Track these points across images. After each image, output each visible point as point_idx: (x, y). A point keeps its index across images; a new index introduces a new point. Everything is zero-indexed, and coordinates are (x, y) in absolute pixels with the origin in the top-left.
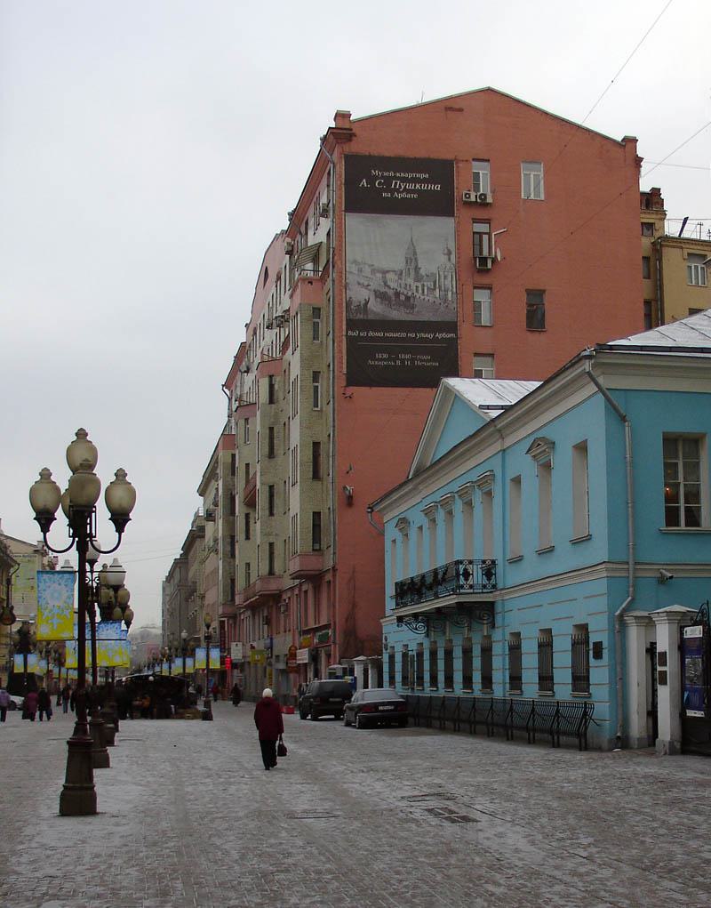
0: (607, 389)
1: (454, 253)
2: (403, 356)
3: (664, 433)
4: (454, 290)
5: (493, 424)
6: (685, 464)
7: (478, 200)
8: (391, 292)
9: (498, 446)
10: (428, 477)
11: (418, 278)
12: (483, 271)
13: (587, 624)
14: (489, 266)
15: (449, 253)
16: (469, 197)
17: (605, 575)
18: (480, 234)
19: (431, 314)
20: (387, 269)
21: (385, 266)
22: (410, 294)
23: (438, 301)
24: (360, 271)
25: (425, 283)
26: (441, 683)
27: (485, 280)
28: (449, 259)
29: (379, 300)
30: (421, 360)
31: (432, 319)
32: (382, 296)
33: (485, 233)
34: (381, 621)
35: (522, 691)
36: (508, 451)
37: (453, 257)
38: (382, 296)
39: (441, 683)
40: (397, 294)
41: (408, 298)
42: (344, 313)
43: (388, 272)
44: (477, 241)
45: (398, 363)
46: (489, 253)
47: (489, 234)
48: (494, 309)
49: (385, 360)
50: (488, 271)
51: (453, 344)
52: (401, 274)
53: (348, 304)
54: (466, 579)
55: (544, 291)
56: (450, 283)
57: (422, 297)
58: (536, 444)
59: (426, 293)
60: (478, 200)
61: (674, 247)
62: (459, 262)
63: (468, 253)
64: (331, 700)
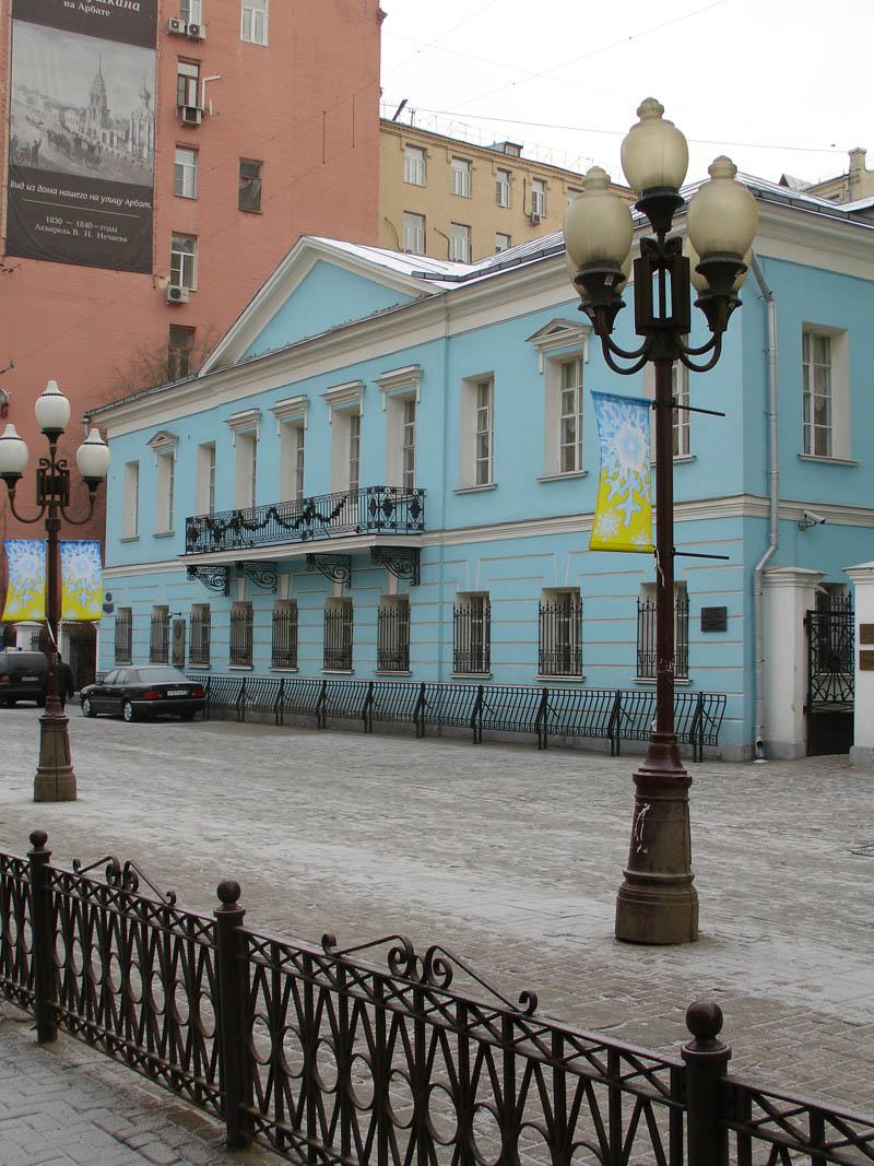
0: (758, 256)
1: (153, 95)
2: (82, 225)
3: (803, 323)
4: (152, 145)
5: (443, 298)
6: (815, 367)
7: (189, 32)
8: (69, 137)
9: (439, 330)
10: (238, 377)
11: (106, 124)
12: (190, 126)
13: (686, 582)
14: (199, 120)
15: (148, 96)
16: (177, 27)
17: (741, 513)
18: (187, 78)
19: (120, 174)
20: (67, 105)
21: (63, 100)
22: (94, 143)
23: (130, 158)
24: (30, 101)
25: (115, 132)
26: (262, 653)
27: (191, 138)
28: (147, 104)
29: (53, 144)
30: (105, 233)
31: (122, 181)
32: (58, 141)
36: (454, 339)
37: (152, 102)
38: (58, 141)
39: (262, 653)
40: (78, 141)
41: (91, 148)
42: (6, 156)
43: (67, 109)
45: (75, 232)
47: (197, 79)
48: (197, 175)
49: (57, 226)
50: (195, 126)
51: (147, 216)
52: (84, 115)
53: (13, 144)
54: (388, 514)
55: (261, 163)
56: (146, 135)
57: (110, 150)
58: (161, 436)
59: (115, 144)
60: (189, 32)
61: (390, 133)
62: (158, 111)
63: (172, 100)
64: (24, 679)
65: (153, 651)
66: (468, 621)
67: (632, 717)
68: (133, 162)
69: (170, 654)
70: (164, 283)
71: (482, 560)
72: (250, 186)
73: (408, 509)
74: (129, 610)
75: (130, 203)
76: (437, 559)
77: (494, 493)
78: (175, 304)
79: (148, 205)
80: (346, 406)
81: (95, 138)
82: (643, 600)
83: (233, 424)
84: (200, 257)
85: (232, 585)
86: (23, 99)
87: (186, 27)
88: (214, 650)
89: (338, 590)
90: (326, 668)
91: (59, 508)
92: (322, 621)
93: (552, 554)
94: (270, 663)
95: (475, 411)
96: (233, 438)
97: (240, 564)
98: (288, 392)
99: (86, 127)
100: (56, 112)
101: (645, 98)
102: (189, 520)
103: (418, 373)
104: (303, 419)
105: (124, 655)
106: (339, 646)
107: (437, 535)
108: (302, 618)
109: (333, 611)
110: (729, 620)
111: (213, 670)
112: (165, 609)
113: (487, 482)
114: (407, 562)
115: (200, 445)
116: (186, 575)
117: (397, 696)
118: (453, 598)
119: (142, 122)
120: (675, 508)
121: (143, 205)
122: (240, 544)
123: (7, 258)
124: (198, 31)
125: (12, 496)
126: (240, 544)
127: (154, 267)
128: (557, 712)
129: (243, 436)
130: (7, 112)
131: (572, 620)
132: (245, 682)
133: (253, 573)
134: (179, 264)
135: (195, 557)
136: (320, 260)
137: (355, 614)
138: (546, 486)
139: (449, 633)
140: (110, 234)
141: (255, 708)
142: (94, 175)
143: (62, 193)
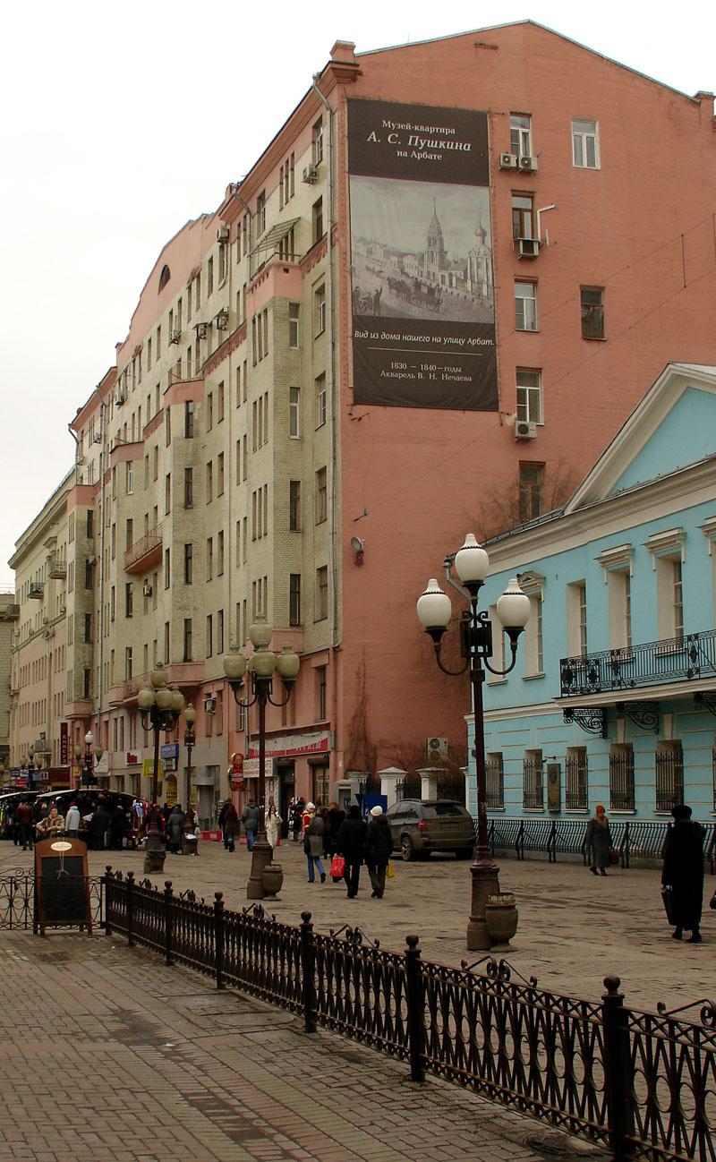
1: (488, 231)
4: (491, 281)
7: (521, 166)
8: (409, 283)
11: (444, 265)
12: (528, 259)
14: (536, 252)
15: (483, 234)
16: (509, 162)
18: (521, 211)
21: (402, 246)
22: (434, 285)
23: (470, 297)
24: (370, 252)
25: (453, 272)
27: (527, 271)
28: (483, 242)
29: (394, 291)
30: (450, 374)
31: (462, 320)
32: (398, 287)
33: (527, 210)
35: (635, 811)
37: (488, 239)
38: (398, 287)
40: (418, 285)
41: (431, 291)
43: (406, 255)
45: (420, 376)
47: (532, 211)
49: (403, 371)
50: (533, 259)
51: (489, 355)
52: (422, 259)
55: (602, 289)
56: (484, 273)
60: (521, 166)
69: (546, 799)
70: (511, 420)
72: (592, 315)
74: (499, 755)
75: (472, 342)
78: (523, 441)
79: (489, 342)
83: (604, 561)
84: (546, 390)
85: (610, 731)
86: (362, 250)
87: (517, 160)
91: (482, 659)
94: (654, 807)
97: (620, 705)
98: (665, 525)
99: (425, 270)
100: (394, 259)
102: (563, 662)
108: (688, 758)
109: (664, 754)
111: (507, 813)
112: (538, 753)
116: (562, 718)
119: (480, 260)
120: (484, 715)
121: (485, 342)
122: (620, 684)
123: (355, 408)
124: (529, 164)
125: (437, 650)
126: (620, 684)
127: (500, 403)
130: (348, 264)
132: (522, 824)
133: (634, 713)
134: (525, 400)
135: (570, 700)
136: (688, 387)
137: (684, 756)
140: (454, 374)
141: (637, 854)
142: (435, 317)
143: (405, 338)
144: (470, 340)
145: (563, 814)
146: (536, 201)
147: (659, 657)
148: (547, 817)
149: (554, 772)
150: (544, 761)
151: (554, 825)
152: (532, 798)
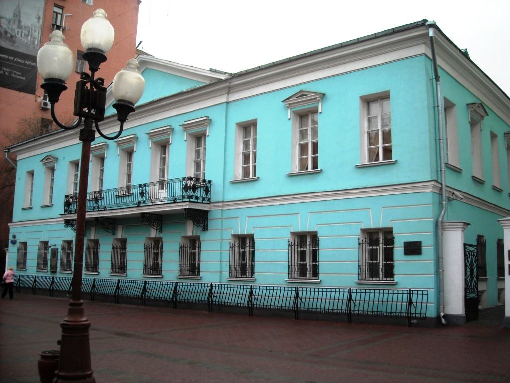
2: (5, 69)
4: (39, 39)
9: (223, 99)
15: (39, 18)
17: (431, 190)
18: (57, 14)
22: (13, 34)
23: (29, 43)
25: (24, 31)
28: (39, 22)
30: (16, 74)
33: (60, 14)
34: (9, 224)
35: (99, 273)
40: (6, 33)
41: (12, 37)
44: (55, 17)
46: (61, 24)
52: (10, 21)
57: (21, 38)
58: (47, 157)
62: (43, 25)
65: (38, 264)
66: (188, 251)
67: (303, 300)
68: (31, 45)
71: (248, 217)
73: (203, 190)
75: (28, 63)
76: (219, 216)
77: (51, 208)
80: (164, 138)
81: (14, 32)
82: (232, 242)
88: (29, 263)
89: (154, 234)
90: (144, 274)
92: (110, 250)
93: (298, 214)
94: (109, 271)
95: (74, 173)
96: (43, 168)
101: (59, 101)
102: (66, 197)
103: (208, 121)
104: (104, 153)
105: (21, 266)
106: (118, 262)
107: (221, 204)
108: (166, 247)
110: (422, 248)
112: (46, 243)
113: (378, 160)
114: (201, 218)
115: (27, 172)
117: (190, 289)
118: (230, 237)
119: (36, 29)
128: (256, 297)
129: (49, 168)
131: (247, 250)
136: (147, 68)
138: (360, 170)
139: (226, 256)
142: (12, 48)
144: (26, 62)
145: (58, 274)
146: (64, 11)
147: (117, 197)
148: (49, 275)
149: (55, 253)
150: (50, 247)
151: (53, 279)
152: (42, 265)
